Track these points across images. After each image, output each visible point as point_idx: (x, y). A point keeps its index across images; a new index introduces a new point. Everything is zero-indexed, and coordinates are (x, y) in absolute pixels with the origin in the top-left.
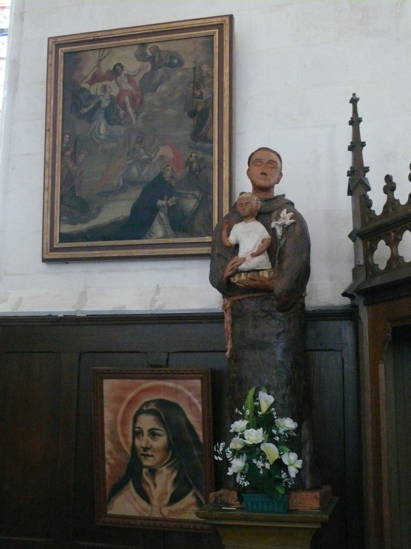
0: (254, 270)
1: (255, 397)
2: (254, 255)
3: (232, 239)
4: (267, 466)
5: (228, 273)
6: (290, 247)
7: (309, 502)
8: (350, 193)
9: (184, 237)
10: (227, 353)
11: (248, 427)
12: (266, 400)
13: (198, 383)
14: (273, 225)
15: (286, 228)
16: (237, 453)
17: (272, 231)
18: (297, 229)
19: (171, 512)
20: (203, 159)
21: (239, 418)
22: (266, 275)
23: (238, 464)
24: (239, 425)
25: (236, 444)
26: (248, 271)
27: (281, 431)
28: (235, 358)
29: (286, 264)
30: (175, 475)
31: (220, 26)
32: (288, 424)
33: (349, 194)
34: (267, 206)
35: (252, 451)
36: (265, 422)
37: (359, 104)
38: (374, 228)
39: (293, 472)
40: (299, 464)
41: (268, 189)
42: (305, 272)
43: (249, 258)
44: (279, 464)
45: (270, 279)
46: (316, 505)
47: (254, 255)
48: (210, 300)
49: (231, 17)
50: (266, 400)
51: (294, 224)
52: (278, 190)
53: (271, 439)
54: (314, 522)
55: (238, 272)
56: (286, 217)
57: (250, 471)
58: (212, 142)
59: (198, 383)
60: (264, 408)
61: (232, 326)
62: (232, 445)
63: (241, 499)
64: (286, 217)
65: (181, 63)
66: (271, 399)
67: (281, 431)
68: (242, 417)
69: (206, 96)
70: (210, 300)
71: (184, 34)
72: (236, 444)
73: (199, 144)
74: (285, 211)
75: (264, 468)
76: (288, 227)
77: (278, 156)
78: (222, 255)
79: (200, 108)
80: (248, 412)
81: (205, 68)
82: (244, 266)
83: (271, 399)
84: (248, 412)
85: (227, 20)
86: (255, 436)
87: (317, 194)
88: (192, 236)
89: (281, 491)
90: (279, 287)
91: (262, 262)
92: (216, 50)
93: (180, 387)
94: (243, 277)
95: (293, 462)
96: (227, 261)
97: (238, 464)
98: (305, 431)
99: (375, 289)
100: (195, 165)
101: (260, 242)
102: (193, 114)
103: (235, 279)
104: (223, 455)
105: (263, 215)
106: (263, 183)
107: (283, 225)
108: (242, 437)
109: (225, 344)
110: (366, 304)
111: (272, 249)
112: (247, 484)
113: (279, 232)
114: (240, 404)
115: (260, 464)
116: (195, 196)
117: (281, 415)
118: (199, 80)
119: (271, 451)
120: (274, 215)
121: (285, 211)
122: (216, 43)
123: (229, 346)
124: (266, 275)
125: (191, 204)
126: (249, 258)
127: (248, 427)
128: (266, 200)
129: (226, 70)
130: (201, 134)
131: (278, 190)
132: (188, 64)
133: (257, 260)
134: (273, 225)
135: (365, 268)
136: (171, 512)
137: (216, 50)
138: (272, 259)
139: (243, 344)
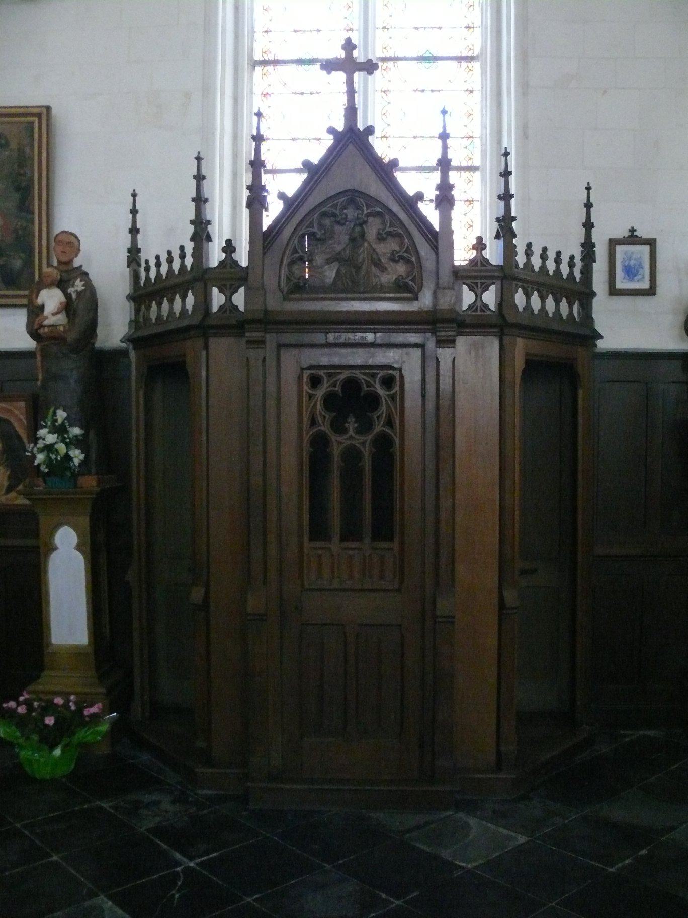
0: (53, 325)
1: (55, 414)
2: (54, 314)
3: (39, 301)
4: (59, 458)
5: (36, 327)
6: (84, 308)
7: (90, 482)
8: (128, 266)
9: (13, 290)
10: (39, 383)
11: (49, 433)
12: (61, 415)
13: (22, 404)
14: (69, 291)
15: (79, 294)
16: (41, 451)
17: (68, 296)
18: (88, 292)
19: (7, 499)
20: (25, 228)
21: (42, 427)
22: (62, 328)
23: (40, 457)
24: (42, 432)
25: (40, 444)
26: (49, 326)
27: (71, 436)
28: (44, 387)
29: (77, 320)
30: (8, 473)
31: (39, 115)
32: (76, 431)
33: (191, 240)
34: (68, 275)
35: (49, 448)
36: (60, 430)
37: (137, 198)
38: (144, 294)
39: (76, 462)
40: (82, 457)
41: (70, 262)
42: (92, 326)
43: (50, 316)
44: (68, 458)
45: (65, 331)
46: (94, 483)
47: (54, 314)
48: (27, 343)
49: (48, 108)
50: (61, 415)
51: (85, 290)
52: (77, 263)
53: (63, 441)
54: (92, 494)
55: (42, 326)
56: (79, 285)
57: (49, 462)
58: (33, 213)
59: (22, 404)
60: (60, 421)
61: (42, 362)
62: (38, 446)
63: (45, 482)
64: (79, 285)
65: (7, 144)
66: (65, 414)
67: (71, 436)
68: (46, 427)
69: (29, 175)
70: (27, 343)
71: (7, 119)
72: (40, 444)
73: (24, 214)
74: (79, 280)
75: (56, 459)
76: (81, 292)
77: (76, 237)
78: (35, 311)
79: (23, 184)
80: (49, 423)
81: (27, 150)
82: (46, 322)
83: (65, 414)
84: (49, 423)
85: (44, 111)
86: (51, 439)
87: (105, 267)
88: (20, 290)
89: (69, 474)
90: (71, 337)
91: (61, 319)
92: (36, 136)
93: (10, 408)
94: (46, 330)
95: (77, 456)
96: (38, 315)
97: (40, 457)
98: (92, 435)
99: (142, 338)
100: (20, 232)
101: (58, 305)
102: (18, 189)
103: (41, 331)
104: (32, 452)
105: (62, 284)
106: (64, 259)
107: (77, 292)
108: (44, 440)
109: (37, 375)
110: (134, 349)
111: (68, 307)
112: (47, 470)
113: (74, 296)
114: (44, 418)
115: (53, 457)
116: (20, 257)
117: (71, 425)
118: (23, 160)
119: (62, 448)
120: (71, 283)
121: (79, 280)
122: (36, 130)
123: (40, 377)
124: (62, 328)
125: (17, 264)
126: (50, 316)
127: (49, 433)
128: (66, 271)
129: (44, 155)
130: (24, 206)
131: (77, 263)
132: (14, 145)
133: (55, 318)
134: (69, 291)
135: (135, 323)
136: (7, 499)
137: (36, 136)
138: (68, 315)
139: (52, 377)
